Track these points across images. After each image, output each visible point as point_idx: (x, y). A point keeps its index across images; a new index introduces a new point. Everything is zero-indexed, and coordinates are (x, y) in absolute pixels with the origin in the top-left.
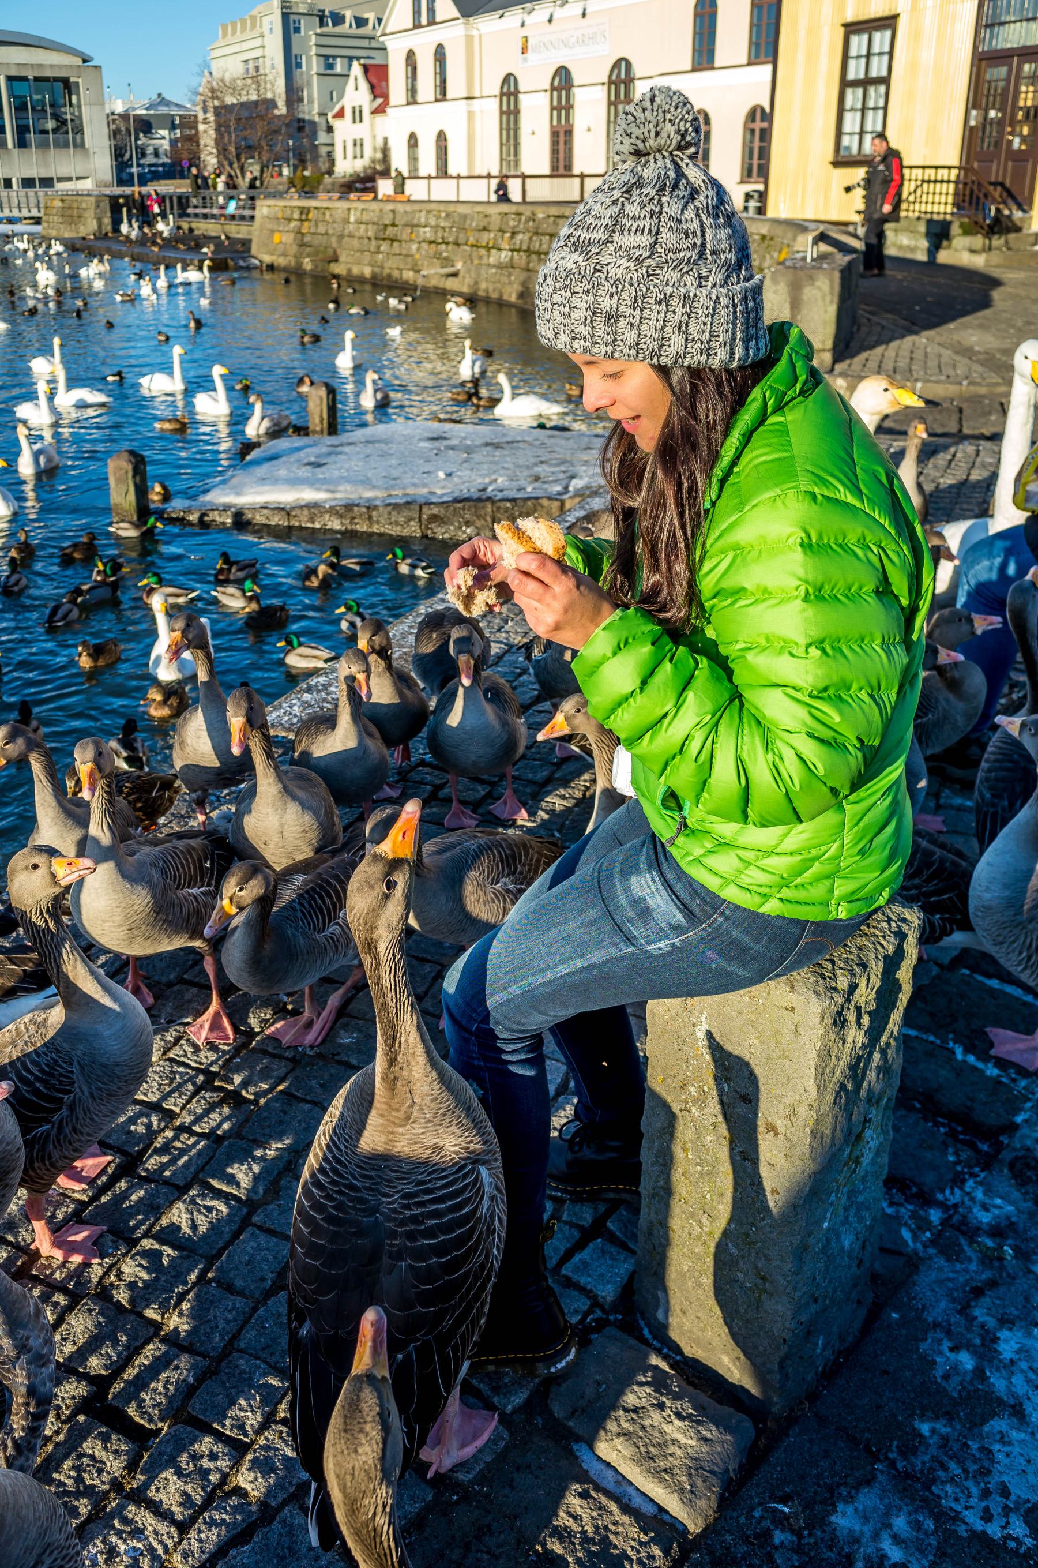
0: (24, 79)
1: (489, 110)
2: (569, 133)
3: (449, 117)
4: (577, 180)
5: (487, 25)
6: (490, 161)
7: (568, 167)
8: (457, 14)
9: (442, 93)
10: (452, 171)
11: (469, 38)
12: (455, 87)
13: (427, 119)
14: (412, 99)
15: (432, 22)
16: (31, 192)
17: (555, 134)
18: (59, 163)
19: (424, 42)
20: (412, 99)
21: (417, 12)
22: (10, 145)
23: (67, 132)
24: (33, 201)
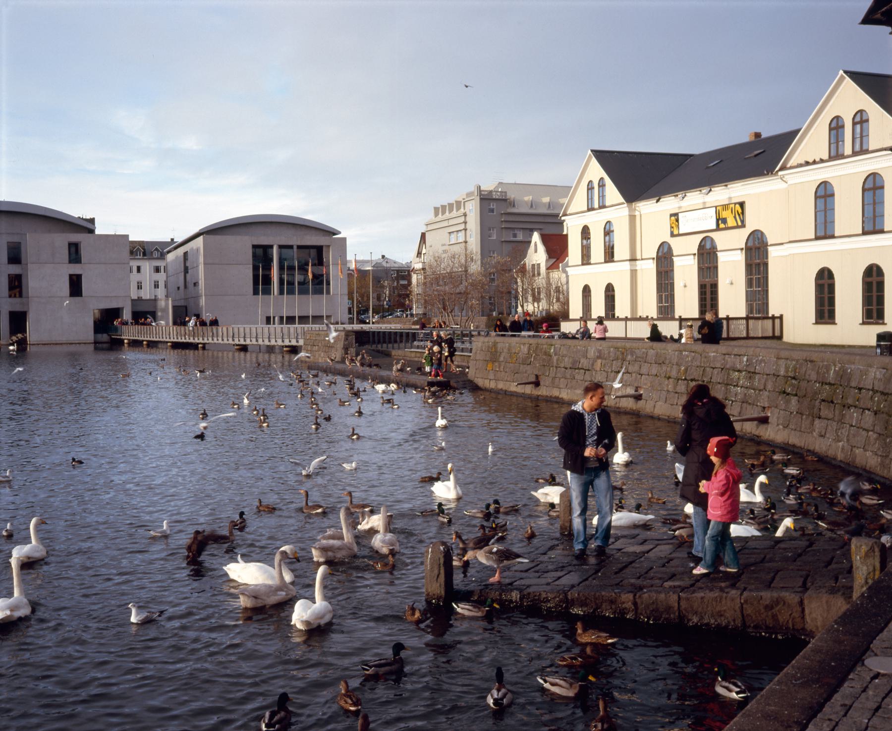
0: (291, 247)
1: (648, 271)
2: (715, 286)
3: (617, 273)
4: (770, 322)
5: (647, 208)
6: (649, 305)
7: (614, 315)
8: (622, 200)
9: (610, 255)
10: (618, 313)
11: (632, 218)
12: (621, 251)
13: (597, 276)
14: (586, 259)
15: (602, 207)
16: (292, 327)
17: (702, 288)
18: (311, 304)
19: (596, 221)
20: (586, 259)
21: (590, 199)
22: (275, 249)
23: (320, 283)
24: (279, 334)
